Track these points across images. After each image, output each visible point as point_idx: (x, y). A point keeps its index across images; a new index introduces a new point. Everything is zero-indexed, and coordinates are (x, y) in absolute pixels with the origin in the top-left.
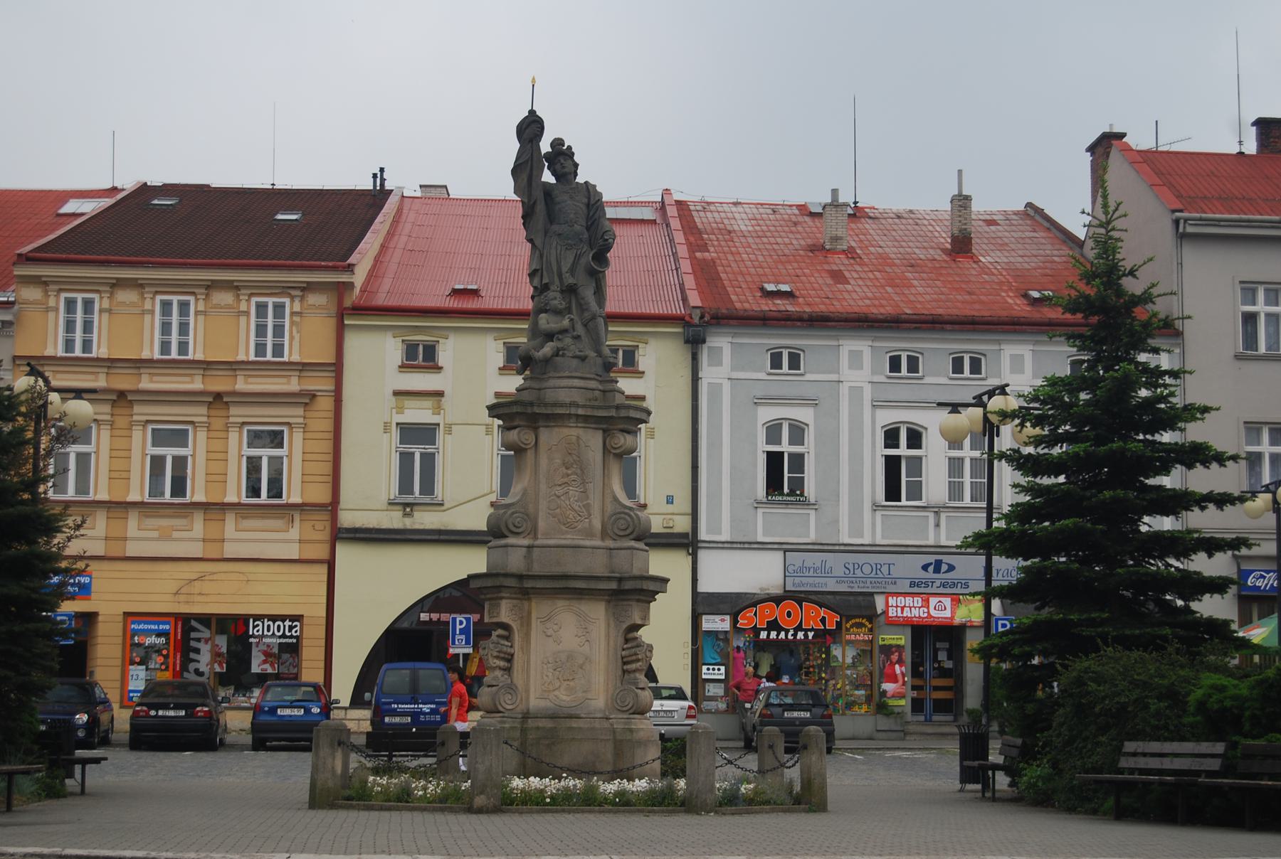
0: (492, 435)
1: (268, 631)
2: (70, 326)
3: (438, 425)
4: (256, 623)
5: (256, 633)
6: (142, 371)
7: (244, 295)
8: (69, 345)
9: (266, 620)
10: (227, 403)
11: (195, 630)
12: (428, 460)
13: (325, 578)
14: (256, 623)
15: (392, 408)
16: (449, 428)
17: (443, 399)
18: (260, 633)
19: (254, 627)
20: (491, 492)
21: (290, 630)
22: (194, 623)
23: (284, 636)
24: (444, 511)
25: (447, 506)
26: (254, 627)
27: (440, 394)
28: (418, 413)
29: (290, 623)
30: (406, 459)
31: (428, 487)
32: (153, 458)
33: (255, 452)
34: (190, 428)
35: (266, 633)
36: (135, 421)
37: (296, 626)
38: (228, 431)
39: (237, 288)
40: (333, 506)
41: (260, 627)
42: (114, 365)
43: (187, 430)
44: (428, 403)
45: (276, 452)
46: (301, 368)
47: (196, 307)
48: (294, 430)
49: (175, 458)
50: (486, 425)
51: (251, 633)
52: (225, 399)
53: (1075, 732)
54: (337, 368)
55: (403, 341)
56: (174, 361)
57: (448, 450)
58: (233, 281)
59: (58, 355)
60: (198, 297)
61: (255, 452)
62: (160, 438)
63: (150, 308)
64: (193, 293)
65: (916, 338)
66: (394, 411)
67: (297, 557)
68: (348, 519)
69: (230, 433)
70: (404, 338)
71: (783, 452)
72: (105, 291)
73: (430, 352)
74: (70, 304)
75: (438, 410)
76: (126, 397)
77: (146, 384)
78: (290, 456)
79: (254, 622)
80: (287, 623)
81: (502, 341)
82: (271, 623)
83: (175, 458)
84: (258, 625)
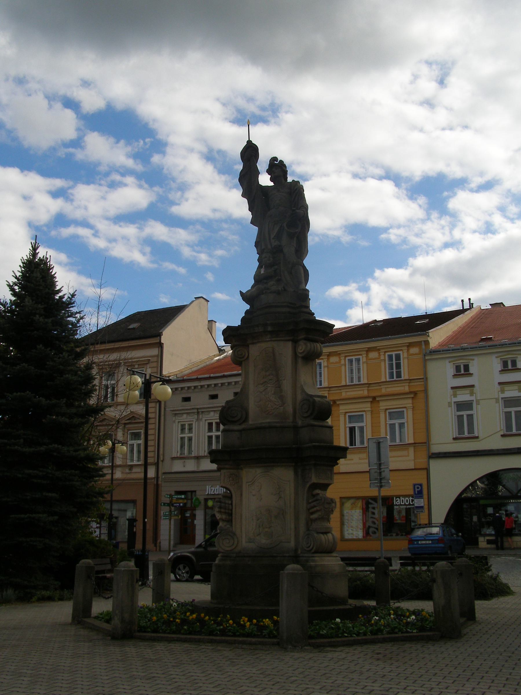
0: (499, 403)
1: (403, 502)
2: (352, 371)
3: (473, 401)
4: (397, 499)
5: (397, 504)
6: (342, 391)
7: (382, 352)
8: (352, 380)
9: (401, 498)
10: (378, 401)
11: (371, 504)
12: (470, 417)
13: (425, 476)
14: (397, 499)
15: (451, 395)
16: (478, 403)
17: (475, 389)
18: (399, 504)
19: (396, 501)
20: (501, 430)
21: (412, 502)
22: (370, 501)
23: (410, 504)
24: (479, 441)
25: (480, 438)
26: (396, 501)
27: (473, 386)
28: (464, 397)
29: (412, 498)
30: (460, 418)
31: (471, 429)
32: (390, 425)
33: (392, 422)
34: (405, 410)
35: (401, 503)
36: (341, 413)
37: (398, 500)
38: (379, 413)
39: (379, 350)
40: (427, 443)
41: (399, 501)
42: (331, 390)
43: (404, 411)
44: (467, 391)
45: (469, 412)
46: (328, 389)
47: (403, 356)
48: (408, 410)
49: (468, 416)
50: (496, 398)
51: (395, 504)
52: (338, 403)
53: (101, 616)
54: (425, 379)
55: (501, 359)
56: (395, 381)
57: (478, 412)
58: (376, 347)
59: (347, 385)
60: (324, 360)
61: (392, 422)
62: (392, 415)
63: (383, 358)
64: (401, 350)
65: (484, 354)
66: (500, 392)
67: (413, 468)
68: (435, 449)
69: (381, 414)
70: (501, 358)
71: (355, 426)
72: (325, 358)
73: (466, 368)
74: (351, 361)
75: (472, 394)
76: (336, 402)
77: (384, 391)
78: (407, 422)
79: (396, 499)
80: (411, 498)
81: (500, 358)
82: (403, 499)
83: (468, 416)
84: (398, 500)
